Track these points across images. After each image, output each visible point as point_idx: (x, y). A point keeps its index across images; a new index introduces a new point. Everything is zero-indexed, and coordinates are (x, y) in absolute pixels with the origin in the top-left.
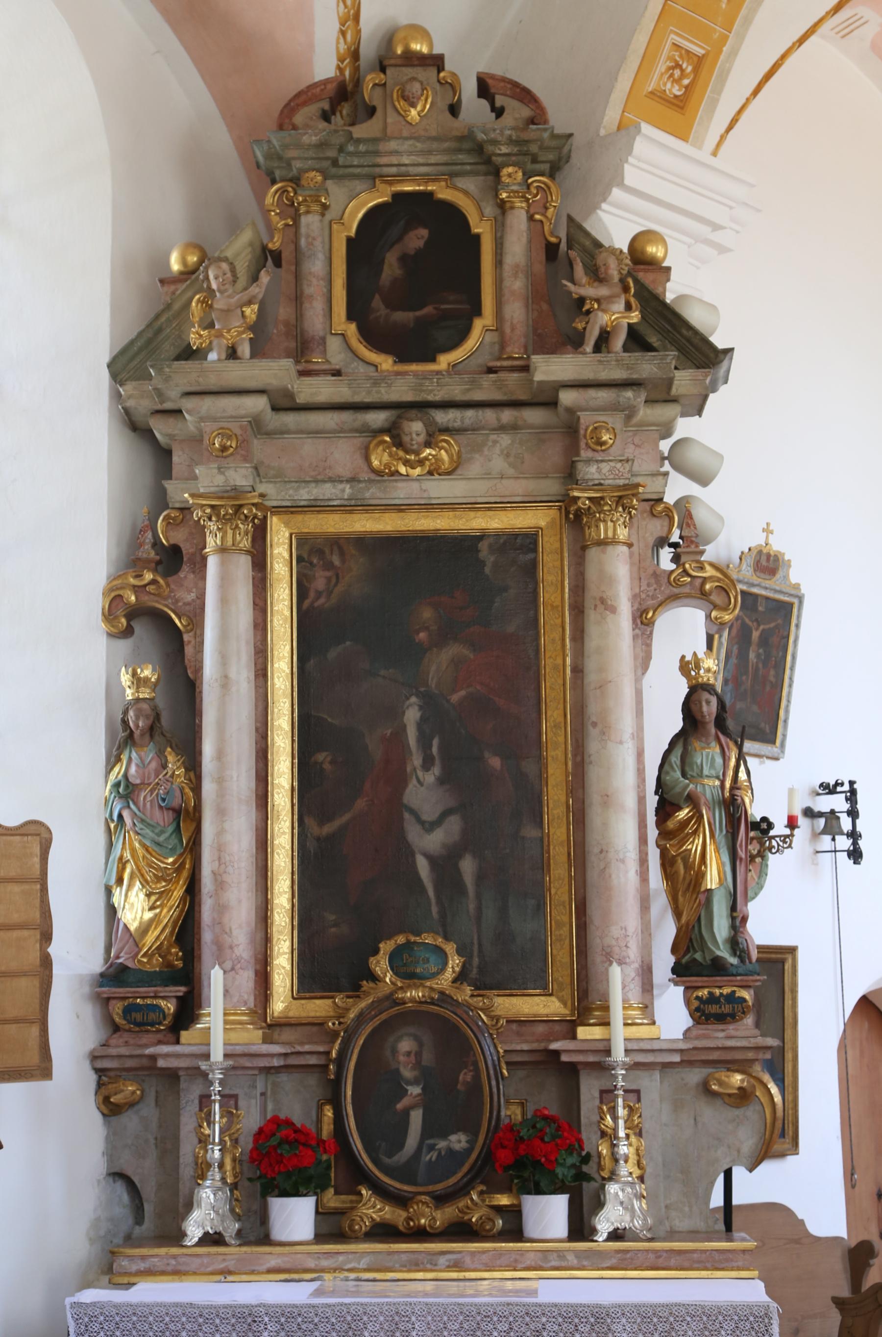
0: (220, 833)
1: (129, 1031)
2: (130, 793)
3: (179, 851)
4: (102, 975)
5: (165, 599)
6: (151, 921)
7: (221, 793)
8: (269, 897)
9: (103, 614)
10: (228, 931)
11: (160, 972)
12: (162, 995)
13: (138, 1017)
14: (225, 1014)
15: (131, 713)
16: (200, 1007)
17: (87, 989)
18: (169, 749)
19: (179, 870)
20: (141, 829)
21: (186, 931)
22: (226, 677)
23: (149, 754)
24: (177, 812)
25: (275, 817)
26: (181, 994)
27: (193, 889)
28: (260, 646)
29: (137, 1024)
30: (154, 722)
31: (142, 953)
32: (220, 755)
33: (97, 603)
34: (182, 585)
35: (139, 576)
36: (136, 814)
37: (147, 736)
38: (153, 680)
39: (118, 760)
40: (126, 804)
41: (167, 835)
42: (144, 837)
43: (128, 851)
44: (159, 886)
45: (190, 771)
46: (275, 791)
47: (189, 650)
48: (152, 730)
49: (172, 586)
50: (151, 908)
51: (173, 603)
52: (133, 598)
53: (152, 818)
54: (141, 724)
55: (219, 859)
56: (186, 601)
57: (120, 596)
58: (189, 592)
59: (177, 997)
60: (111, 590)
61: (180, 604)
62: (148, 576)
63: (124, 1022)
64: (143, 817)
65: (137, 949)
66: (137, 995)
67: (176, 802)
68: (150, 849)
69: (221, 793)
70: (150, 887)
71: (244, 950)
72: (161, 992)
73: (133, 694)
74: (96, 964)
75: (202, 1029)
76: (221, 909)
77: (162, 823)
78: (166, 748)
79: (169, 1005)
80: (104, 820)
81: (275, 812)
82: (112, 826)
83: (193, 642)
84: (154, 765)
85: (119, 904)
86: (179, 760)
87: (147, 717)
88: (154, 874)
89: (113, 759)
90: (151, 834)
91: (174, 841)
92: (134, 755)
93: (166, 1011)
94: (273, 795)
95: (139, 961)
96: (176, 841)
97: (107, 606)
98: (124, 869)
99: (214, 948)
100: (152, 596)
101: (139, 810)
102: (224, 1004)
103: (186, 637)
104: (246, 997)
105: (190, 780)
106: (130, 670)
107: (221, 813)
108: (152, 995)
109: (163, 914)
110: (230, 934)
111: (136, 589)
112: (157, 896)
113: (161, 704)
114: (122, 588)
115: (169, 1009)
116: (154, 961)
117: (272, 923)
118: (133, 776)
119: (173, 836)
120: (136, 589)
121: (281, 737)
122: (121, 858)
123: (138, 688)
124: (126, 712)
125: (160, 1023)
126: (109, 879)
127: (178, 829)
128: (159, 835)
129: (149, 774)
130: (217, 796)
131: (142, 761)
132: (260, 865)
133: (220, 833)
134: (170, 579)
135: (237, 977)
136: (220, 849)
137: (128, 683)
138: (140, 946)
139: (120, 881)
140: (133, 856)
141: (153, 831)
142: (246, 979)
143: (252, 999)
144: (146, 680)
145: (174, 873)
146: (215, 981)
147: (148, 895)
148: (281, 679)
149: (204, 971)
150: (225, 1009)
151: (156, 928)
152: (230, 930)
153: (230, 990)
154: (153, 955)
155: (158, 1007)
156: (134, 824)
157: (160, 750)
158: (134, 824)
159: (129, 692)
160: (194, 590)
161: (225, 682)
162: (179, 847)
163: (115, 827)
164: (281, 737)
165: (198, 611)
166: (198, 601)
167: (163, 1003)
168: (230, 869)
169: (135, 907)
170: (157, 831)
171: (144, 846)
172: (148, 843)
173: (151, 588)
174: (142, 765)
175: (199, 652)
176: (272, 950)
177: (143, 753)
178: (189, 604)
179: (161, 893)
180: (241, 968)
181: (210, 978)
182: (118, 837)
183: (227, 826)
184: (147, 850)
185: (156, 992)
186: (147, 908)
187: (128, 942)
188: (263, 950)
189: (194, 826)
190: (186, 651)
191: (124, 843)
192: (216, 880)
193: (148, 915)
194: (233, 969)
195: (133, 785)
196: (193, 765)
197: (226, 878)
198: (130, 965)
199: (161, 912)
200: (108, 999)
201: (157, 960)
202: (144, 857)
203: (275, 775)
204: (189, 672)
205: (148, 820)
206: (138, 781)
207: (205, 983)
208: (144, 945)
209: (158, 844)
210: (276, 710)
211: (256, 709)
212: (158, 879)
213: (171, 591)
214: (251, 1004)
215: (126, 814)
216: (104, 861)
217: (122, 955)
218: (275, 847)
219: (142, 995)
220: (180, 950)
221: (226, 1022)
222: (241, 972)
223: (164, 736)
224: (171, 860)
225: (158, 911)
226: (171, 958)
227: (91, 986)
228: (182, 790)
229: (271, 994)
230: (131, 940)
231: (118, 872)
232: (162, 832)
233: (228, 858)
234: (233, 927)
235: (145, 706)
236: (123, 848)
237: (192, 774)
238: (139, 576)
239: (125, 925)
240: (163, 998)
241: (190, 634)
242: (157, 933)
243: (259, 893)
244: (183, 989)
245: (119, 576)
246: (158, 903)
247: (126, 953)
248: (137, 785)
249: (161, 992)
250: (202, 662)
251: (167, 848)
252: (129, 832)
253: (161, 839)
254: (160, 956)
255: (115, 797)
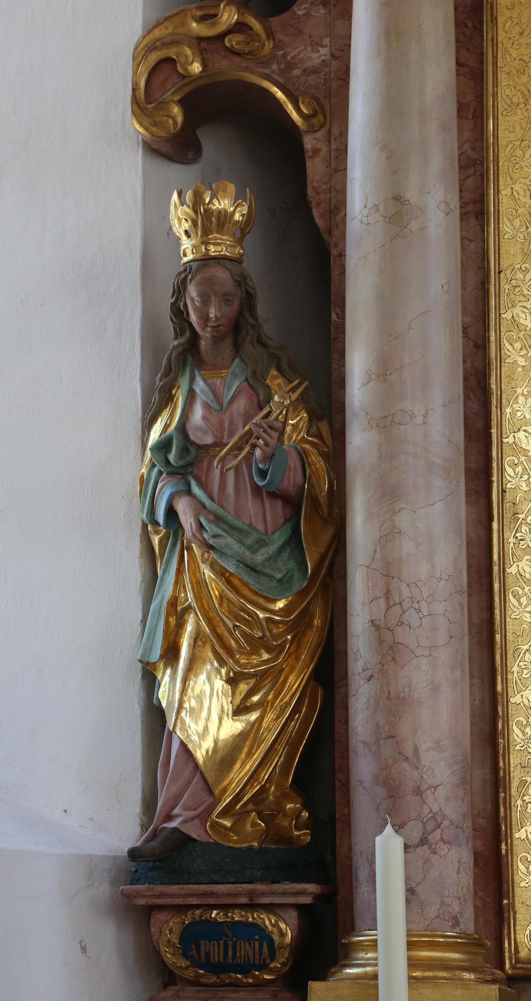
0: (388, 537)
1: (196, 983)
2: (190, 464)
3: (299, 584)
4: (133, 854)
5: (266, 63)
6: (242, 737)
7: (390, 449)
8: (499, 688)
9: (135, 100)
10: (410, 754)
11: (261, 851)
12: (265, 900)
13: (215, 951)
14: (411, 945)
15: (192, 291)
16: (352, 929)
17: (103, 890)
18: (274, 372)
19: (299, 624)
20: (215, 536)
21: (316, 759)
22: (398, 198)
23: (233, 382)
24: (292, 503)
25: (508, 515)
26: (307, 900)
27: (329, 673)
28: (470, 153)
29: (216, 969)
30: (241, 313)
31: (220, 808)
32: (385, 369)
33: (120, 79)
34: (301, 32)
35: (208, 18)
36: (204, 506)
37: (228, 343)
38: (237, 217)
39: (167, 399)
40: (182, 487)
41: (272, 549)
42: (222, 554)
43: (189, 587)
44: (255, 660)
45: (320, 419)
46: (507, 460)
47: (315, 169)
48: (239, 330)
49: (279, 36)
50: (240, 710)
51: (281, 72)
52: (196, 68)
53: (238, 515)
54: (212, 313)
55: (388, 593)
56: (309, 64)
57: (169, 61)
58: (316, 44)
59: (299, 907)
60: (151, 48)
61: (297, 72)
62: (229, 16)
63: (184, 963)
64: (220, 511)
65: (211, 800)
66: (212, 901)
67: (291, 479)
68: (236, 581)
69: (390, 449)
70: (237, 662)
71: (447, 799)
72: (263, 894)
73: (194, 247)
74: (123, 832)
75: (357, 977)
76: (394, 704)
77: (260, 527)
78: (267, 370)
79: (283, 926)
80: (140, 524)
81: (507, 505)
82: (156, 540)
83: (325, 150)
84: (241, 404)
85: (170, 703)
86: (293, 390)
87: (226, 298)
88: (245, 635)
89: (157, 400)
90: (236, 546)
91: (286, 565)
92: (200, 385)
93: (276, 938)
94: (502, 470)
95: (216, 826)
96: (291, 564)
97: (142, 84)
98: (180, 625)
99: (381, 792)
100: (237, 59)
101: (212, 498)
102: (408, 922)
103: (309, 142)
104: (456, 907)
105: (319, 436)
106: (189, 196)
107: (390, 493)
108: (244, 900)
109: (265, 724)
110: (415, 758)
111: (202, 44)
112: (252, 681)
113: (252, 268)
114: (173, 43)
115: (282, 935)
116: (249, 828)
117: (507, 747)
118: (199, 429)
119: (286, 554)
120: (202, 44)
121: (518, 345)
122: (173, 603)
123: (206, 232)
124: (180, 291)
125: (263, 967)
126: (148, 650)
127: (295, 541)
128: (253, 549)
129: (232, 423)
130: (380, 457)
131: (217, 397)
132: (476, 620)
133: (388, 537)
134: (275, 21)
135: (435, 859)
136: (388, 572)
137: (186, 226)
138: (216, 792)
139: (171, 653)
140: (198, 597)
141: (241, 542)
142: (454, 866)
143: (470, 912)
144: (224, 219)
145: (287, 632)
146: (387, 856)
147: (232, 681)
148: (517, 222)
149: (359, 846)
150: (409, 934)
151: (250, 754)
152: (416, 750)
153: (418, 889)
154: (244, 812)
155: (257, 929)
156: (201, 527)
157: (254, 373)
158: (201, 527)
159: (186, 244)
160: (326, 41)
161: (397, 212)
162: (297, 576)
163: (162, 537)
164: (518, 345)
165: (334, 85)
166: (335, 64)
167: (268, 921)
168: (412, 617)
169: (208, 714)
170: (249, 541)
171: (221, 573)
172: (230, 567)
173: (232, 41)
174: (218, 406)
175: (337, 171)
176: (508, 807)
177: (218, 382)
178: (315, 71)
179: (260, 677)
180: (442, 839)
181: (372, 862)
182: (168, 562)
183: (403, 521)
184: (228, 582)
185: (251, 894)
186: (229, 708)
187: (189, 782)
188: (489, 807)
189: (330, 531)
190: (309, 171)
191: (180, 571)
192: (381, 642)
193: (233, 727)
194: (423, 841)
195: (200, 447)
196: (326, 406)
197: (402, 634)
198: (194, 836)
199: (260, 720)
200: (150, 909)
201: (254, 824)
202: (221, 597)
203: (506, 426)
204: (315, 213)
205: (230, 518)
206: (209, 440)
207: (362, 875)
208: (224, 790)
209: (252, 569)
210: (505, 287)
211: (463, 288)
212: (256, 645)
213: (277, 46)
214: (468, 924)
215: (183, 507)
216: (140, 616)
217: (176, 811)
218: (509, 581)
219: (220, 899)
220: (305, 806)
221: (412, 964)
222: (443, 849)
223: (265, 346)
224: (280, 604)
225: (253, 716)
226: (285, 823)
227: (114, 882)
228: (303, 457)
229: (512, 905)
230: (198, 776)
231: (166, 633)
232: (261, 543)
233: (406, 593)
234: (423, 747)
235: (221, 274)
236: (178, 580)
237: (324, 427)
238: (208, 18)
239: (183, 745)
240: (270, 908)
241: (318, 135)
242: (250, 766)
243: (477, 681)
244: (312, 888)
245: (167, 19)
246: (255, 698)
247: (185, 808)
248: (206, 447)
249: (263, 894)
250: (343, 191)
251: (271, 577)
252: (190, 549)
253: (259, 557)
254: (260, 816)
255: (160, 473)
